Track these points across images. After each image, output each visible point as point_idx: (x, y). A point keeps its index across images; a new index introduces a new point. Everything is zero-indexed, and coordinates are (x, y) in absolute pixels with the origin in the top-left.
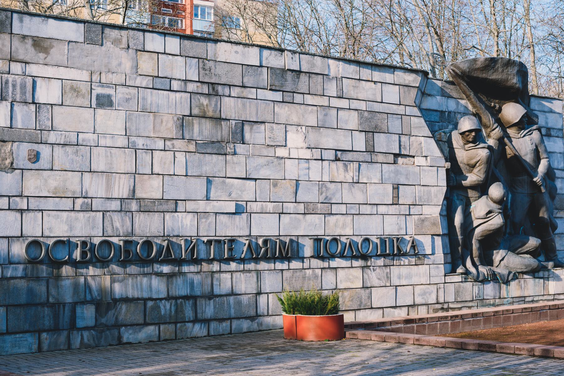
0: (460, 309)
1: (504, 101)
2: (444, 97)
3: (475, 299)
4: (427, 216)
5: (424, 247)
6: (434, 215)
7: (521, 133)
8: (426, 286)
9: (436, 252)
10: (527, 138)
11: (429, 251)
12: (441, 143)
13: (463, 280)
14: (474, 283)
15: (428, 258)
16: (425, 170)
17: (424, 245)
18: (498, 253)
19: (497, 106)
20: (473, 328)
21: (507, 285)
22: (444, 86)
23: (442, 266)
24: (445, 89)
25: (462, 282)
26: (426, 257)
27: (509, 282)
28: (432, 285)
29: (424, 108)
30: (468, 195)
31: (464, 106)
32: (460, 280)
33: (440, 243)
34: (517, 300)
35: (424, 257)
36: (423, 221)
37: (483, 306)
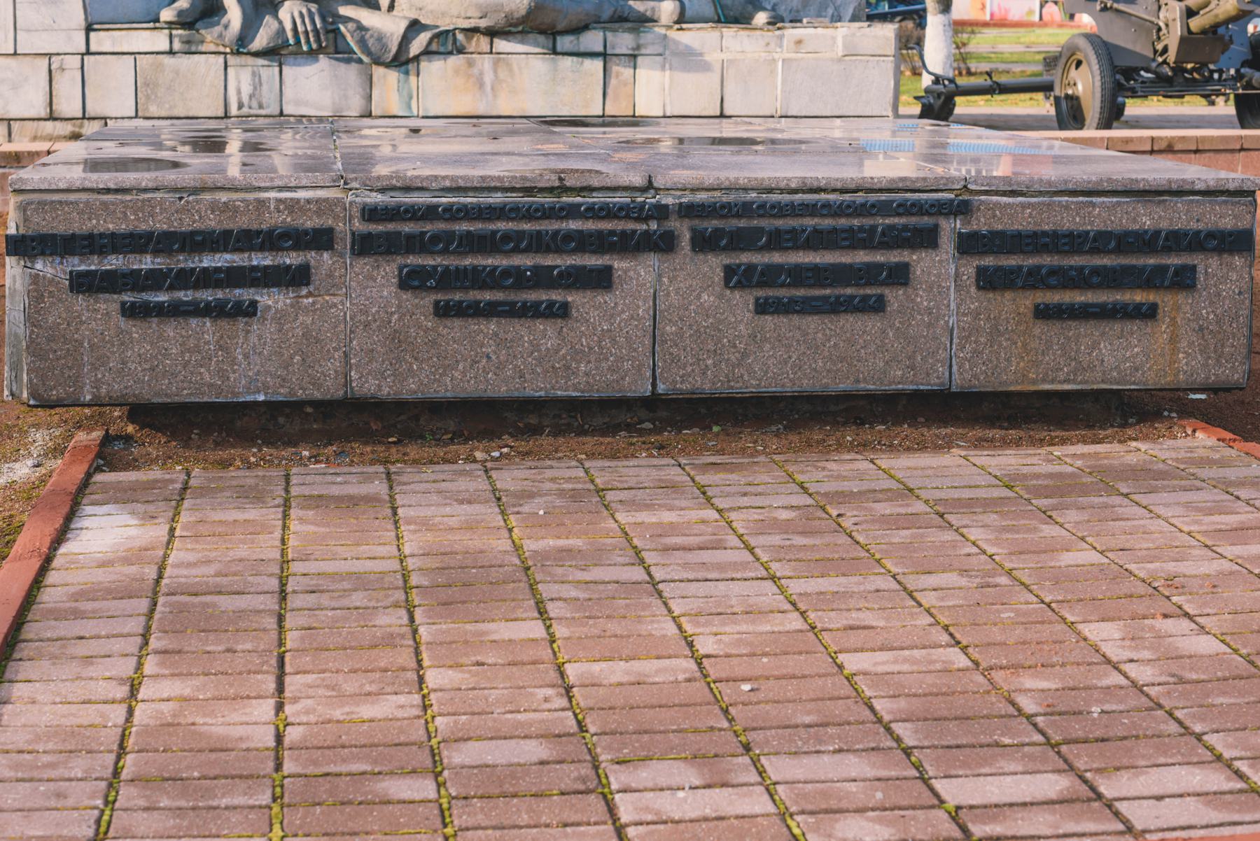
3: (234, 110)
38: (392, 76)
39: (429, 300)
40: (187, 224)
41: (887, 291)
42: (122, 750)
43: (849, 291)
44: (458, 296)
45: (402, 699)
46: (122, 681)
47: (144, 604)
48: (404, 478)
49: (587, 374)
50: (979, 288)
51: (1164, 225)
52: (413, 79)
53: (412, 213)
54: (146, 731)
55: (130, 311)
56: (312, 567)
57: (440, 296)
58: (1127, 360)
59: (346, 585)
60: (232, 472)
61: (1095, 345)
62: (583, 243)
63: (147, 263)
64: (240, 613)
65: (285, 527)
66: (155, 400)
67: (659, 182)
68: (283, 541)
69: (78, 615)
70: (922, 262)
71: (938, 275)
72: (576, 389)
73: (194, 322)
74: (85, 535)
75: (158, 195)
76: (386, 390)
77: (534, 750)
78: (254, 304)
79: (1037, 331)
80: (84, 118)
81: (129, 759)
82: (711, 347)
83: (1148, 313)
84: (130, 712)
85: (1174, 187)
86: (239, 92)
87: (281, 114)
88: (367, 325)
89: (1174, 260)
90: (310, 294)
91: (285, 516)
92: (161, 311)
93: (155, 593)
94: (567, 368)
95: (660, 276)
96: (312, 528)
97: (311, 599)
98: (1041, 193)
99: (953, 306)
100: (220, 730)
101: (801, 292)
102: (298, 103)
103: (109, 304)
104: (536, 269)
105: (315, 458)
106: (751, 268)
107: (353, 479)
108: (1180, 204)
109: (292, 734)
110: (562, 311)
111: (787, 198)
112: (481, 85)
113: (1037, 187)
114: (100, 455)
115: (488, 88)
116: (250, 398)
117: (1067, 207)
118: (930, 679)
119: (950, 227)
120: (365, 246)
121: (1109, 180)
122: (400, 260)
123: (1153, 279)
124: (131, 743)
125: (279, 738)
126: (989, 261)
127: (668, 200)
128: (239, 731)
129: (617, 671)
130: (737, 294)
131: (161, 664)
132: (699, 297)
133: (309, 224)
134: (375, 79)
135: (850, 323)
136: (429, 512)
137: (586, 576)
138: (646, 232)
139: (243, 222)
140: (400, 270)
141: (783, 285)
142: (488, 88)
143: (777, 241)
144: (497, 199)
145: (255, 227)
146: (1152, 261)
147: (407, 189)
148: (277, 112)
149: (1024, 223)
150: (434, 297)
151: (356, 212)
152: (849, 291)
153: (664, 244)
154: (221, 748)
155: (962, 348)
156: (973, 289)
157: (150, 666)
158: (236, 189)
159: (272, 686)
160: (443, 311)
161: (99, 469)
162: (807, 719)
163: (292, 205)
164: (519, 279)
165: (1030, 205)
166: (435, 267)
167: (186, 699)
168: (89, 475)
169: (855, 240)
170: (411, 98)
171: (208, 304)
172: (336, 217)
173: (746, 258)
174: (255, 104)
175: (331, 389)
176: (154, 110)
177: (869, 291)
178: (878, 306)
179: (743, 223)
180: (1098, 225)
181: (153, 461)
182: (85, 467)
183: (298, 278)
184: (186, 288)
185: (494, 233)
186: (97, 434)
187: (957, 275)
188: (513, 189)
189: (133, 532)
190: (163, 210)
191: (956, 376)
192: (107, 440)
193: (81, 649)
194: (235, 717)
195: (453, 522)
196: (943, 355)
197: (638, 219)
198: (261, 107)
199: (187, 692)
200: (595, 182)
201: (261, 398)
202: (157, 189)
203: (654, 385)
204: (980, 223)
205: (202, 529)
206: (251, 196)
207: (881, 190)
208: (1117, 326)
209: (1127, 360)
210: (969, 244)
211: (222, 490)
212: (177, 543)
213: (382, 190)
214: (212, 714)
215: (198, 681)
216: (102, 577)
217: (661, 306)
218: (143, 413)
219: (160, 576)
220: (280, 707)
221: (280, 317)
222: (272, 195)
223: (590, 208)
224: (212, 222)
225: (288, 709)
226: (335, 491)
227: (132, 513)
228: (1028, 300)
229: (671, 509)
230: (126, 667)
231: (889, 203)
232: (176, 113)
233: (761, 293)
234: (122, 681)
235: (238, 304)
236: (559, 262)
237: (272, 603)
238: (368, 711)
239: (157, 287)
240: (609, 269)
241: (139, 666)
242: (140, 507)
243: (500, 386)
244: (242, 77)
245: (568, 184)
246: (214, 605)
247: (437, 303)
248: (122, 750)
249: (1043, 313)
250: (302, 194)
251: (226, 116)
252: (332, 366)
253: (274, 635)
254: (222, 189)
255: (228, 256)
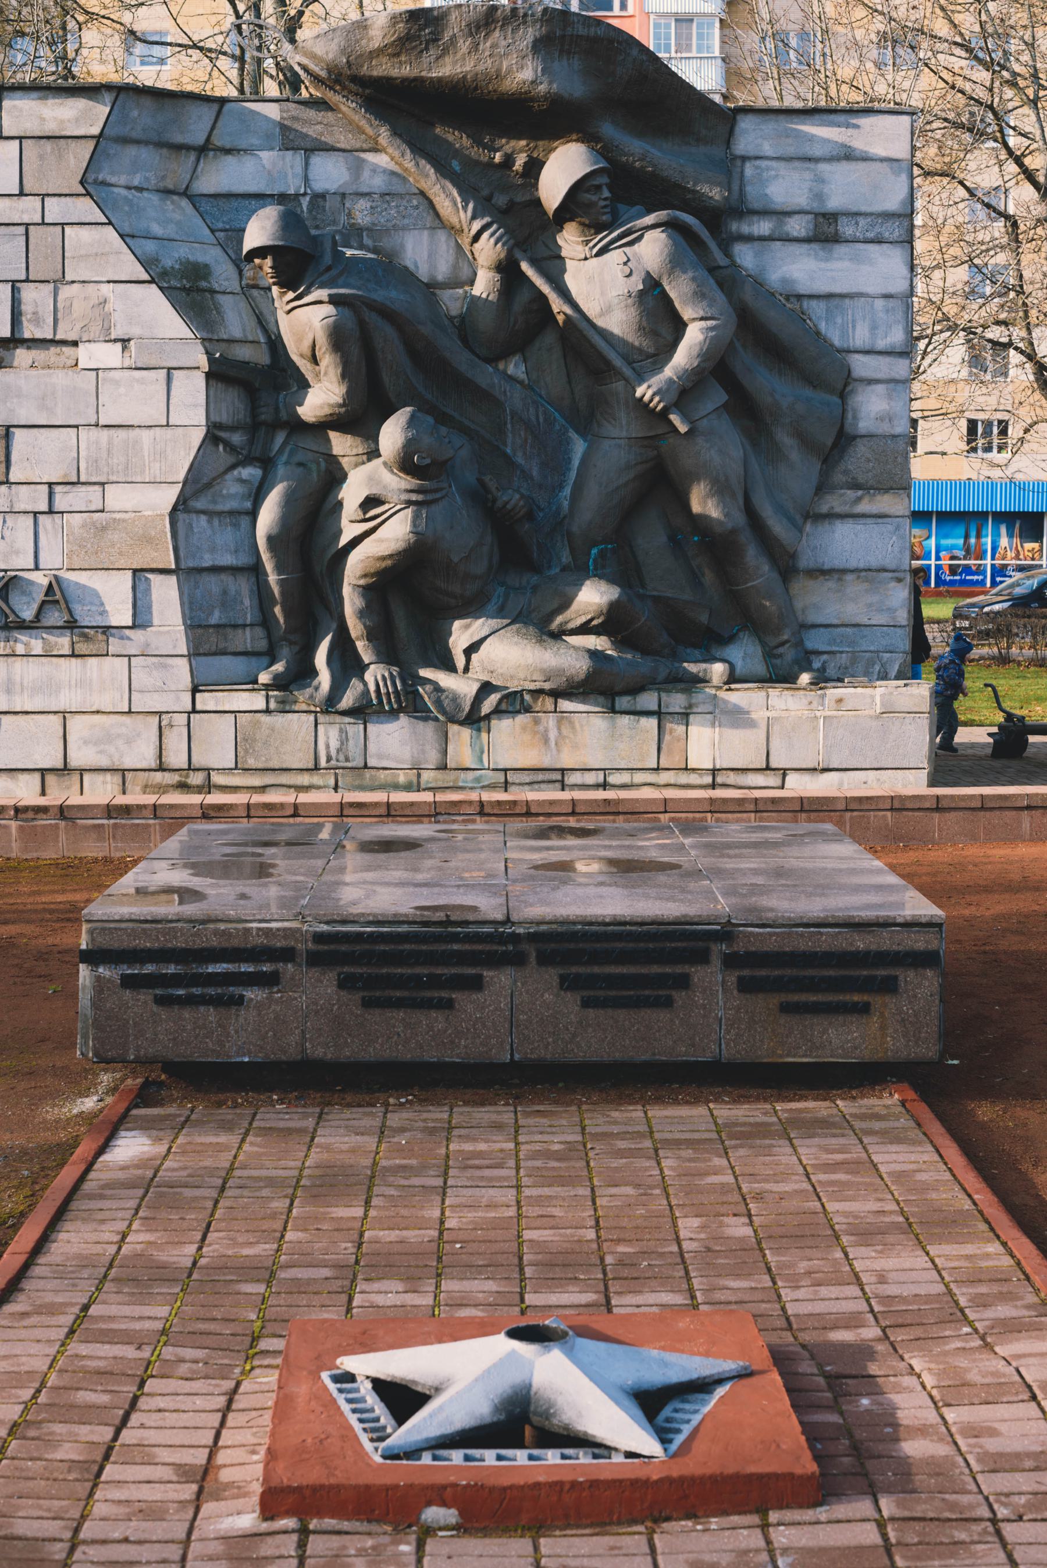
0: (263, 789)
1: (546, 142)
2: (290, 153)
3: (323, 763)
4: (117, 516)
5: (102, 604)
6: (146, 513)
7: (591, 244)
8: (112, 716)
9: (156, 622)
10: (615, 256)
11: (121, 615)
12: (255, 292)
13: (273, 705)
14: (321, 718)
15: (122, 638)
16: (117, 383)
17: (105, 600)
18: (467, 627)
19: (520, 161)
20: (117, 849)
21: (479, 730)
22: (295, 119)
23: (183, 665)
24: (297, 126)
25: (267, 711)
26: (113, 635)
27: (488, 717)
28: (141, 716)
29: (205, 192)
30: (331, 448)
31: (385, 171)
32: (261, 705)
33: (174, 594)
34: (526, 777)
35: (104, 633)
36: (104, 529)
37: (362, 788)
38: (466, 733)
39: (358, 996)
40: (198, 944)
41: (674, 993)
42: (111, 1266)
43: (647, 992)
44: (378, 994)
45: (267, 1246)
46: (118, 1233)
47: (140, 1192)
48: (329, 1117)
49: (466, 1047)
50: (739, 991)
51: (873, 947)
52: (484, 735)
53: (347, 937)
54: (126, 1257)
55: (160, 1001)
56: (245, 1173)
57: (365, 994)
58: (848, 1041)
59: (262, 1184)
60: (223, 1110)
61: (825, 1031)
62: (463, 958)
63: (171, 969)
64: (195, 1199)
65: (240, 1147)
66: (177, 1060)
67: (514, 918)
68: (235, 1157)
69: (102, 1197)
70: (699, 974)
71: (710, 982)
72: (458, 1056)
73: (202, 1009)
74: (117, 1150)
75: (180, 925)
76: (329, 1056)
77: (326, 1272)
78: (242, 997)
79: (782, 1021)
80: (189, 769)
81: (114, 1270)
82: (551, 1030)
83: (864, 1009)
84: (120, 1248)
85: (881, 920)
86: (328, 747)
87: (366, 767)
88: (317, 1012)
89: (882, 972)
90: (279, 991)
91: (243, 1140)
92: (181, 1001)
93: (149, 1186)
94: (452, 1042)
95: (515, 981)
96: (256, 1149)
97: (238, 1192)
98: (783, 926)
99: (721, 1003)
100: (165, 1258)
101: (613, 993)
102: (380, 757)
103: (146, 996)
104: (430, 976)
105: (281, 1101)
106: (578, 976)
107: (296, 1117)
108: (885, 933)
109: (203, 1262)
110: (448, 1005)
111: (603, 928)
112: (546, 741)
113: (780, 921)
114: (138, 1096)
115: (553, 744)
116: (239, 1059)
117: (802, 935)
118: (568, 1245)
119: (719, 949)
120: (315, 960)
121: (833, 916)
122: (339, 969)
123: (869, 985)
124: (116, 1263)
125: (195, 1263)
126: (746, 972)
127: (521, 931)
128: (175, 1259)
129: (393, 1235)
130: (569, 994)
131: (142, 1225)
132: (542, 996)
133: (279, 945)
134: (450, 735)
135: (648, 1014)
136: (332, 1140)
137: (406, 1183)
138: (504, 952)
139: (235, 943)
140: (339, 975)
141: (601, 988)
142: (553, 744)
143: (596, 958)
144: (404, 929)
145: (243, 946)
146: (865, 973)
147: (344, 922)
148: (362, 764)
149: (771, 946)
150: (361, 994)
151: (309, 937)
152: (647, 992)
153: (517, 960)
154: (163, 1266)
155: (728, 1032)
156: (735, 992)
157: (135, 1226)
158: (231, 921)
159: (199, 1237)
160: (368, 1004)
161: (137, 1106)
162: (481, 1263)
163: (268, 932)
164: (416, 982)
165: (775, 934)
166: (362, 975)
167: (150, 1243)
168: (128, 1110)
169: (649, 957)
170: (482, 752)
171: (211, 996)
172: (297, 940)
173: (574, 969)
174: (342, 757)
175: (292, 1054)
176: (252, 763)
177: (661, 993)
178: (667, 1003)
179: (572, 946)
180: (825, 947)
181: (174, 1101)
182: (125, 1104)
183: (270, 980)
184: (197, 986)
185: (402, 951)
186: (139, 1081)
187: (723, 981)
188: (415, 923)
189: (146, 1149)
190: (182, 935)
191: (724, 1052)
192: (146, 1084)
193: (100, 1216)
194: (175, 1252)
195: (345, 1147)
196: (714, 1037)
197: (500, 943)
198: (347, 760)
199: (152, 1239)
200: (471, 917)
201: (246, 1060)
202: (178, 921)
203: (512, 1055)
204: (740, 947)
205: (189, 1148)
206: (240, 926)
207: (669, 924)
208: (841, 1018)
209: (848, 1041)
210: (731, 961)
211: (208, 1122)
212: (171, 1156)
213: (327, 923)
214: (163, 1251)
215: (158, 1234)
216: (121, 1175)
217: (516, 1001)
218: (169, 1067)
219: (155, 1176)
220: (200, 1248)
221: (259, 1006)
222: (255, 925)
223: (467, 935)
224: (214, 942)
225: (204, 1249)
226: (282, 1124)
227: (149, 1136)
228: (775, 1000)
229: (486, 1141)
230: (122, 1226)
231: (674, 932)
232: (271, 765)
233: (586, 993)
234: (118, 1233)
235: (232, 997)
236: (446, 971)
237: (214, 1194)
238: (246, 1251)
239: (178, 986)
240: (480, 977)
241: (130, 1225)
242: (154, 1133)
243: (407, 1054)
244: (330, 735)
245: (452, 919)
246: (181, 1194)
247: (363, 998)
248: (111, 1266)
249: (787, 1008)
250: (274, 925)
251: (316, 768)
252: (294, 1039)
253: (209, 1211)
254: (221, 921)
255: (225, 965)
